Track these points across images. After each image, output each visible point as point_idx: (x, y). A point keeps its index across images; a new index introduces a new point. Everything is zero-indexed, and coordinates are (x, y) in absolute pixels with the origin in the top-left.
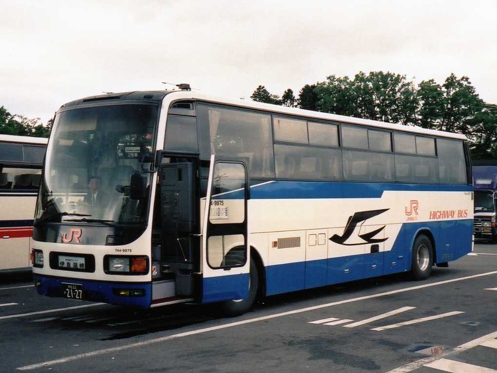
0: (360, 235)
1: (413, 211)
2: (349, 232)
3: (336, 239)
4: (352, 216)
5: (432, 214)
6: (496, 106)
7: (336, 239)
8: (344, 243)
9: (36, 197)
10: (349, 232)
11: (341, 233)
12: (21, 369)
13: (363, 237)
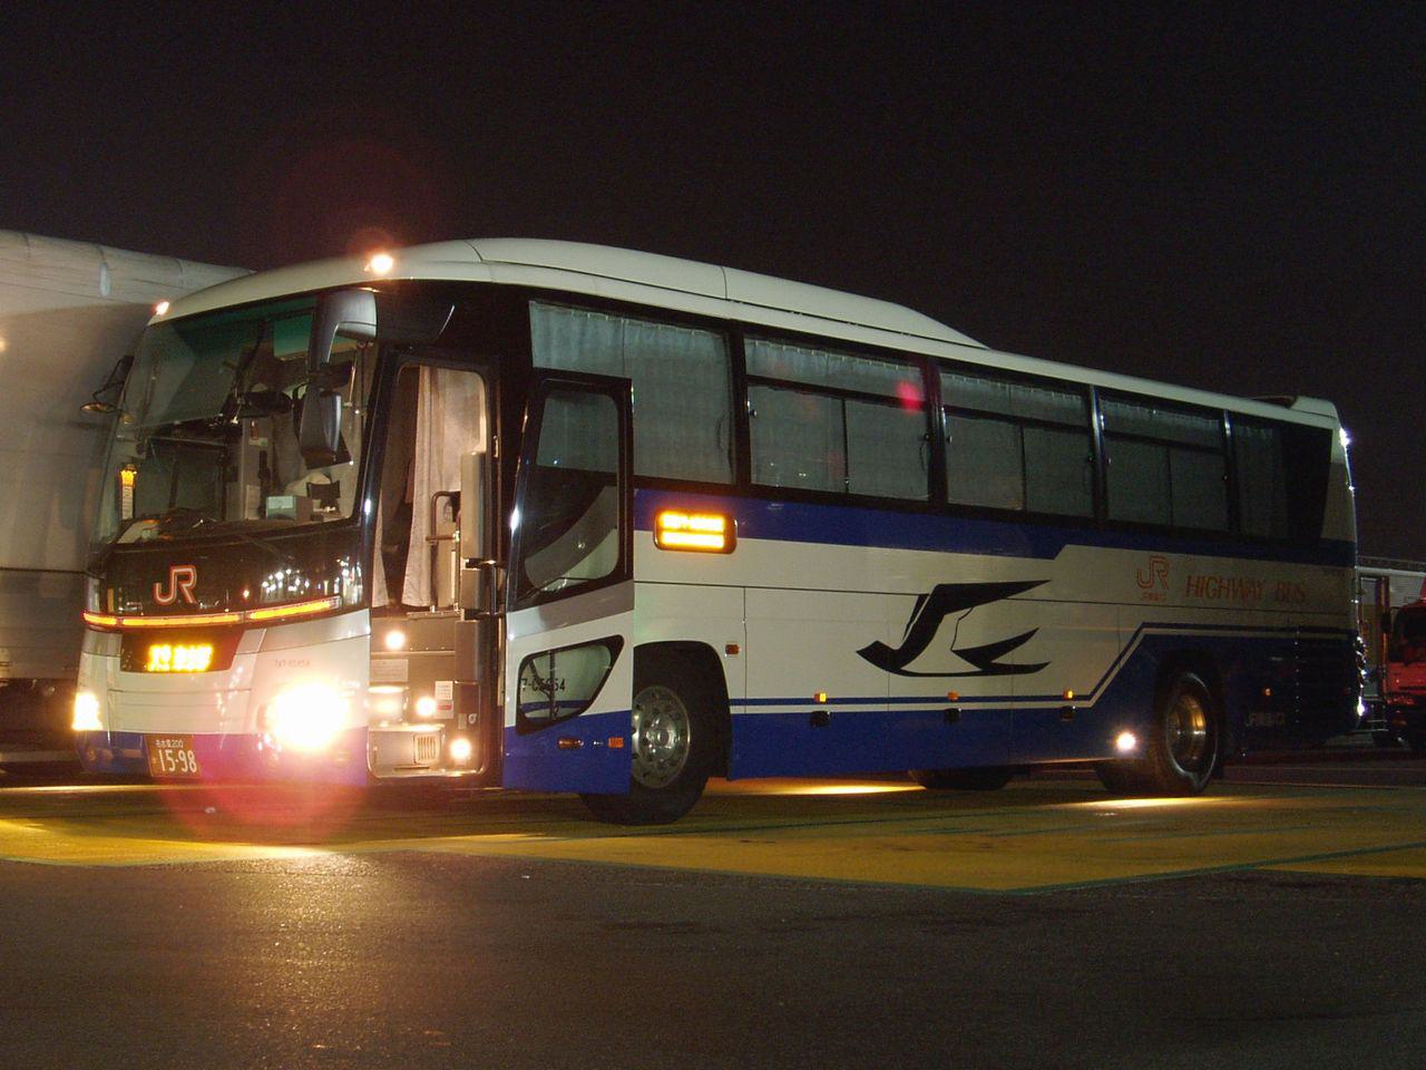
0: (958, 647)
1: (1157, 580)
2: (920, 636)
3: (877, 654)
4: (927, 595)
5: (1193, 582)
6: (1423, 688)
7: (877, 654)
8: (905, 668)
9: (923, 495)
10: (920, 636)
11: (895, 641)
12: (583, 714)
13: (964, 654)
